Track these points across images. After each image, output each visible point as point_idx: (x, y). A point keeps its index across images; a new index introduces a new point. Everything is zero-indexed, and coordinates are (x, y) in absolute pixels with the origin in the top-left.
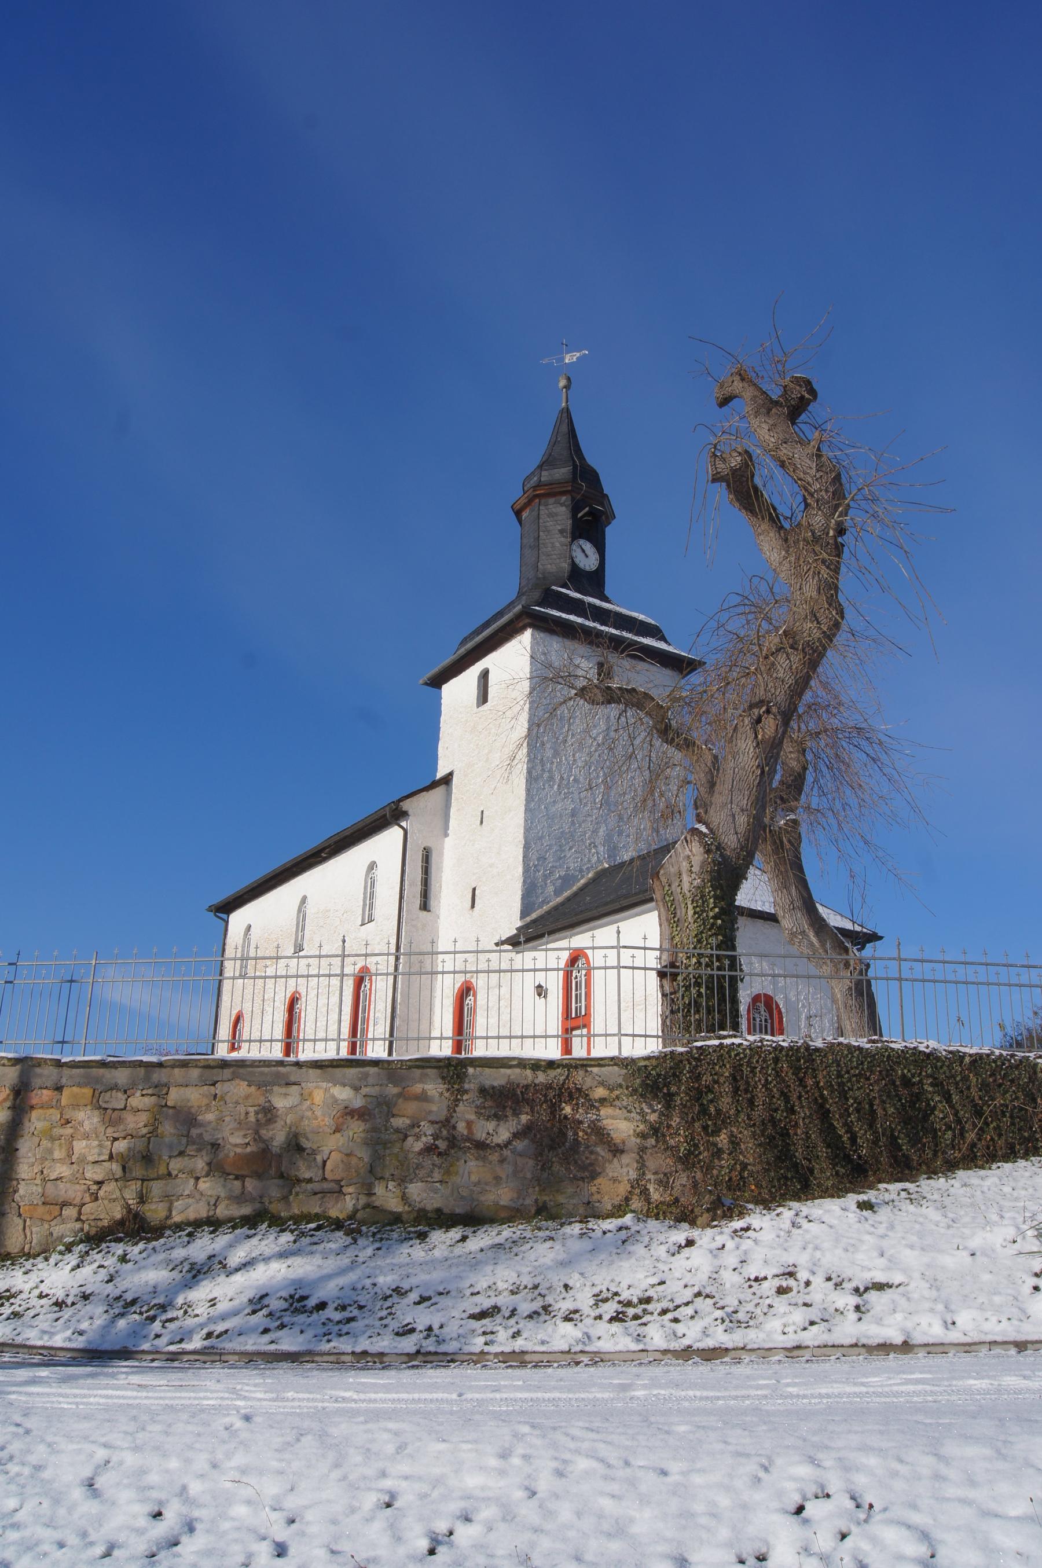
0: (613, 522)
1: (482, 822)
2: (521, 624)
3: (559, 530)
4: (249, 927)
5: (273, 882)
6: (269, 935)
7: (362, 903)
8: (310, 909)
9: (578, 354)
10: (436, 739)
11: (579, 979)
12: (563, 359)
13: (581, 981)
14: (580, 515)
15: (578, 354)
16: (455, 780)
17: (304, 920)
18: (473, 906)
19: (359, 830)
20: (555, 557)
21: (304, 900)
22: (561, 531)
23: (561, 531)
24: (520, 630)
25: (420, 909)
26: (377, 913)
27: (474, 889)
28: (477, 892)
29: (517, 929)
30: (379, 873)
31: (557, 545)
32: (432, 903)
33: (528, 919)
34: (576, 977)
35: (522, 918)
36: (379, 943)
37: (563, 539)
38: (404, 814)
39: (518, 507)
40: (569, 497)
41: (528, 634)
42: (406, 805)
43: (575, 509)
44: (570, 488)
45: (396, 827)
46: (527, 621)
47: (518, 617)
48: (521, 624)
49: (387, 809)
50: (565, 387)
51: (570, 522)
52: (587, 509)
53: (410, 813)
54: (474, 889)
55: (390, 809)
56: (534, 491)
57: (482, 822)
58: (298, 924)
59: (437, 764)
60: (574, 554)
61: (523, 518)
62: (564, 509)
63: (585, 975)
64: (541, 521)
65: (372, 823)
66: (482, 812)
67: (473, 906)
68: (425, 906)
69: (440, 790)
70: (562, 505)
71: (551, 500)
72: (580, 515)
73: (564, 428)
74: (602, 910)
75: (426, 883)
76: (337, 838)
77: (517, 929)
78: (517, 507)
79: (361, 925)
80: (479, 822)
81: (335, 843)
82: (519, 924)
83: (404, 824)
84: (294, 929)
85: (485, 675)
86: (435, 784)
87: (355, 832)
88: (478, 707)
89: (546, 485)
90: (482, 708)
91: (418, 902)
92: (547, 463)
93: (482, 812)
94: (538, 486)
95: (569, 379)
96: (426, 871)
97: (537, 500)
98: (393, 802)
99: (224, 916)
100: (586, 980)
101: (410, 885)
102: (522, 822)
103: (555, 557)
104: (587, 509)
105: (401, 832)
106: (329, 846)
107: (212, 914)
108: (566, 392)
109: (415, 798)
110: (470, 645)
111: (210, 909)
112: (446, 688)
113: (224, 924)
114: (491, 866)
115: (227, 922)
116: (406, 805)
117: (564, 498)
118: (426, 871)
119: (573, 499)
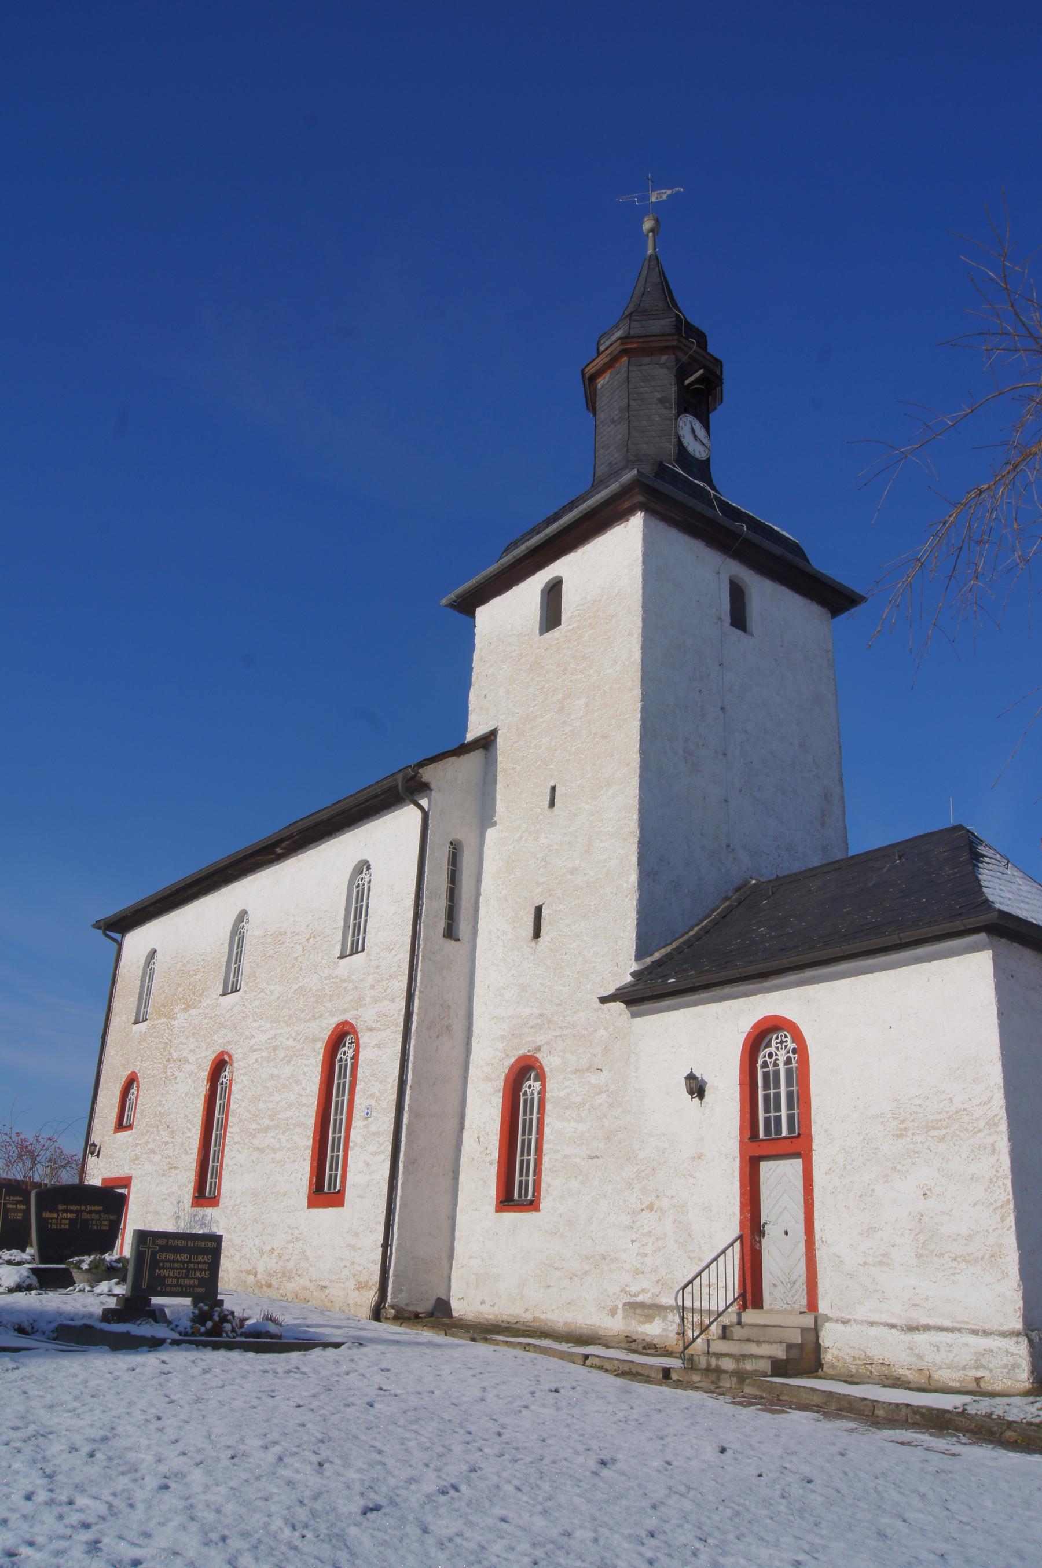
0: (719, 408)
1: (552, 804)
2: (627, 505)
3: (659, 399)
4: (154, 952)
5: (195, 890)
6: (184, 965)
7: (342, 923)
8: (253, 932)
9: (669, 192)
10: (468, 684)
11: (343, 1063)
12: (648, 197)
13: (346, 1065)
14: (687, 382)
15: (669, 192)
16: (500, 741)
17: (151, 979)
18: (537, 934)
19: (343, 812)
20: (653, 433)
21: (242, 916)
22: (662, 401)
23: (662, 401)
24: (629, 512)
25: (444, 936)
26: (373, 937)
27: (539, 910)
28: (544, 913)
29: (632, 974)
30: (378, 876)
31: (657, 418)
32: (463, 928)
33: (648, 960)
34: (341, 1060)
35: (639, 957)
36: (372, 987)
37: (664, 411)
38: (424, 788)
39: (593, 370)
40: (673, 357)
41: (637, 521)
42: (427, 774)
43: (682, 373)
44: (675, 343)
45: (412, 806)
46: (640, 498)
47: (625, 492)
48: (627, 505)
49: (400, 776)
50: (652, 230)
51: (674, 389)
52: (701, 372)
53: (433, 786)
54: (539, 910)
55: (404, 777)
56: (622, 344)
57: (552, 804)
58: (142, 986)
59: (467, 719)
60: (681, 433)
61: (599, 386)
62: (665, 371)
63: (352, 1059)
64: (631, 386)
65: (367, 801)
66: (553, 789)
67: (537, 934)
68: (450, 933)
69: (474, 758)
70: (663, 366)
71: (647, 360)
72: (687, 382)
73: (655, 278)
74: (958, 925)
75: (452, 895)
76: (307, 823)
77: (632, 974)
78: (591, 370)
79: (341, 957)
80: (547, 803)
81: (300, 832)
82: (634, 967)
83: (424, 803)
84: (225, 959)
85: (553, 592)
86: (464, 749)
87: (334, 816)
88: (541, 633)
89: (639, 337)
90: (548, 635)
91: (441, 925)
92: (637, 313)
93: (553, 789)
94: (626, 338)
95: (657, 221)
96: (454, 877)
97: (625, 359)
98: (411, 766)
99: (117, 936)
100: (352, 1064)
101: (430, 898)
102: (634, 802)
103: (653, 433)
104: (701, 372)
105: (418, 815)
106: (290, 837)
107: (100, 932)
108: (654, 236)
109: (440, 765)
110: (522, 549)
111: (97, 925)
112: (485, 615)
113: (115, 946)
114: (572, 871)
115: (120, 945)
116: (427, 774)
117: (664, 358)
118: (454, 877)
119: (677, 360)
